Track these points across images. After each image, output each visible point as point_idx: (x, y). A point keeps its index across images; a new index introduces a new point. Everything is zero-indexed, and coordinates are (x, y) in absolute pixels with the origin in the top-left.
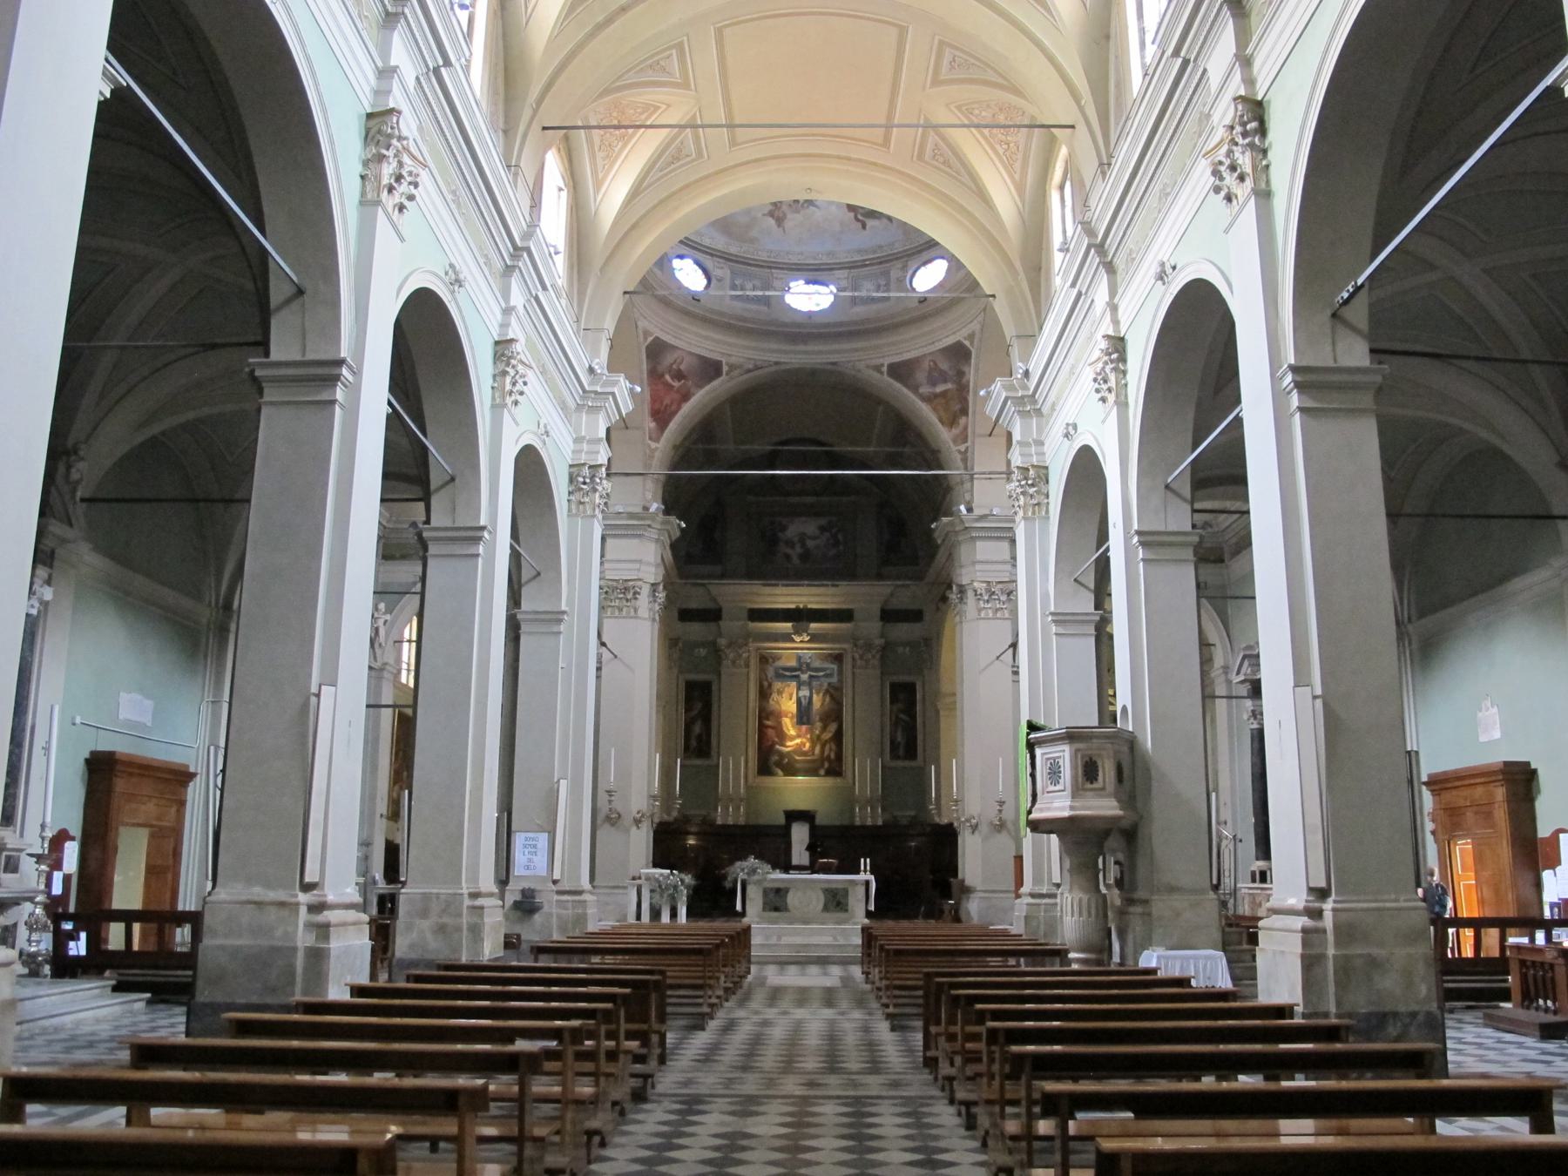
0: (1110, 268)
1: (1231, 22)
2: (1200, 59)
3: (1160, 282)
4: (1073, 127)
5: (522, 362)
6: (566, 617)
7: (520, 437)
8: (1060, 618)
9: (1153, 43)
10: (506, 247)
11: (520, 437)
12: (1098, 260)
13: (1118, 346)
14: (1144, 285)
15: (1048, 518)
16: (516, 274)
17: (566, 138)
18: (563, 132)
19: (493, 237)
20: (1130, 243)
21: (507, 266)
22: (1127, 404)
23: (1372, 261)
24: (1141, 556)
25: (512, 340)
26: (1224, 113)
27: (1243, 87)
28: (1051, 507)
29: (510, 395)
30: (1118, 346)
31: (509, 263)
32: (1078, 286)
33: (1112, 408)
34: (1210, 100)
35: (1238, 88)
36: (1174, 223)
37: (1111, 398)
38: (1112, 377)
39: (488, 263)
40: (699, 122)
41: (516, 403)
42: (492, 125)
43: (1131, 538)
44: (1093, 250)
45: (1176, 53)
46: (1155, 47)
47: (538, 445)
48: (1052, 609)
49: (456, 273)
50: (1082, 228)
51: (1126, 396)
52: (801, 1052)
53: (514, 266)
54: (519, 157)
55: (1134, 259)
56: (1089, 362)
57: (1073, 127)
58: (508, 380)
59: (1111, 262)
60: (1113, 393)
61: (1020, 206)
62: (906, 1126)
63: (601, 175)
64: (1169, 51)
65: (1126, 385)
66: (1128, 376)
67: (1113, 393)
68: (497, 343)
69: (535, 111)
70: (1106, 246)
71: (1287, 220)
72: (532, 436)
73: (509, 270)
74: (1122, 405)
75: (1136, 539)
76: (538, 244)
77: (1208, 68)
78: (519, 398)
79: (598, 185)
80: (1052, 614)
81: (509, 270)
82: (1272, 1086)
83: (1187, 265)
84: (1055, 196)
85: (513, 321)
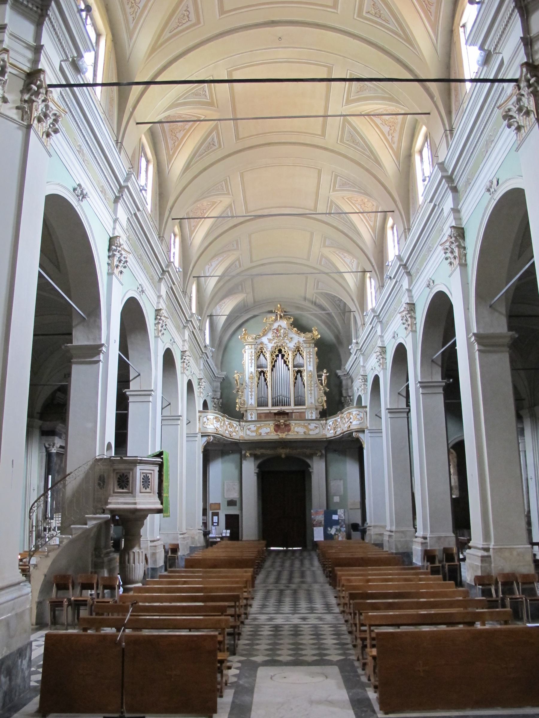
0: (455, 190)
1: (407, 278)
2: (400, 282)
3: (488, 193)
4: (393, 211)
5: (165, 317)
6: (153, 393)
7: (127, 292)
8: (371, 431)
9: (422, 195)
10: (159, 271)
11: (127, 292)
12: (403, 271)
13: (412, 307)
14: (471, 205)
15: (386, 369)
16: (121, 201)
17: (180, 222)
18: (179, 220)
19: (84, 136)
20: (416, 266)
21: (160, 278)
22: (466, 265)
23: (506, 285)
24: (421, 392)
25: (161, 309)
26: (447, 231)
27: (454, 222)
28: (418, 325)
29: (161, 331)
30: (412, 307)
31: (185, 325)
32: (434, 202)
33: (456, 268)
34: (443, 221)
35: (406, 299)
36: (474, 196)
37: (409, 328)
38: (456, 250)
39: (103, 191)
40: (235, 215)
41: (163, 334)
42: (109, 118)
43: (470, 338)
44: (401, 267)
45: (431, 201)
46: (423, 198)
47: (138, 298)
48: (420, 380)
49: (142, 288)
50: (438, 167)
51: (386, 366)
52: (276, 606)
53: (186, 326)
54: (164, 233)
55: (419, 272)
56: (440, 243)
57: (393, 211)
58: (116, 259)
59: (409, 272)
60: (457, 260)
61: (374, 238)
62: (322, 635)
63: (131, 26)
64: (428, 200)
65: (416, 324)
66: (417, 320)
67: (457, 260)
68: (156, 310)
69: (170, 212)
70: (407, 265)
71: (472, 271)
72: (134, 292)
73: (117, 200)
74: (463, 265)
75: (419, 385)
76: (172, 269)
77: (403, 285)
78: (123, 270)
79: (169, 161)
80: (420, 382)
81: (117, 200)
82: (466, 611)
83: (506, 181)
84: (389, 232)
85: (161, 301)
